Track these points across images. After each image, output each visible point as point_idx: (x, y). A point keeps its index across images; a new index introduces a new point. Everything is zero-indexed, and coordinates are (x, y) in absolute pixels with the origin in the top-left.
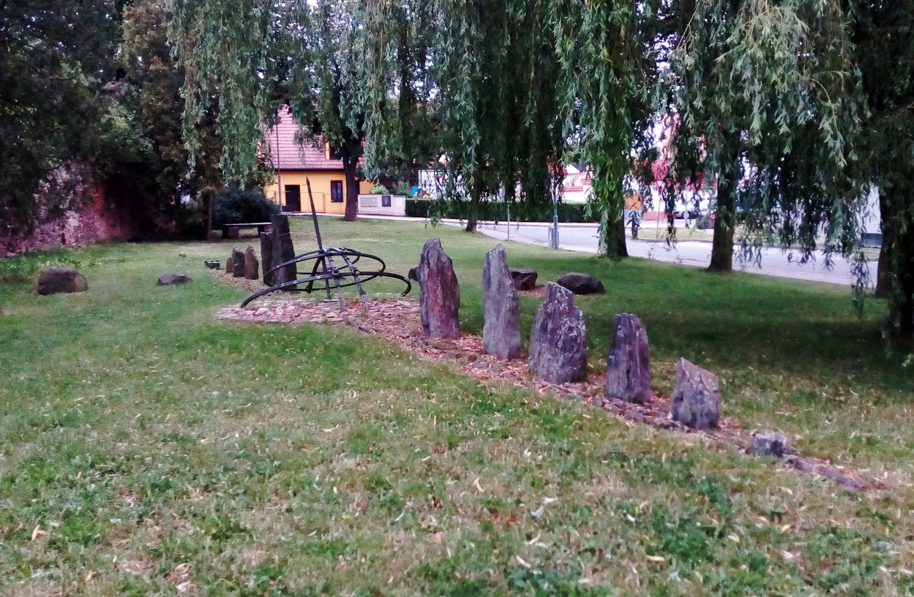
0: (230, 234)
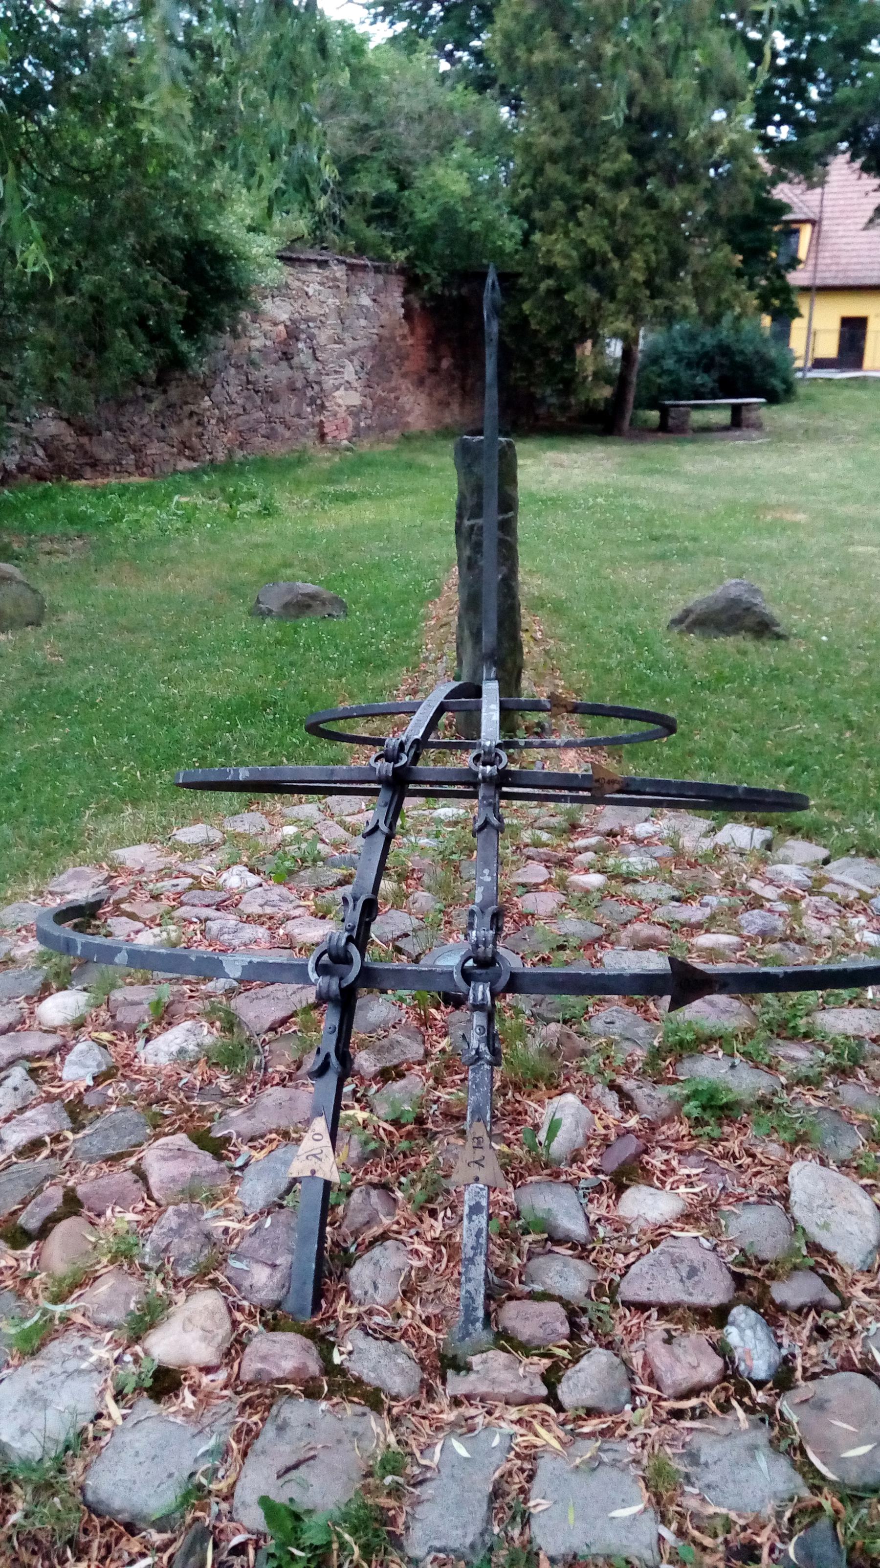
0: (671, 422)
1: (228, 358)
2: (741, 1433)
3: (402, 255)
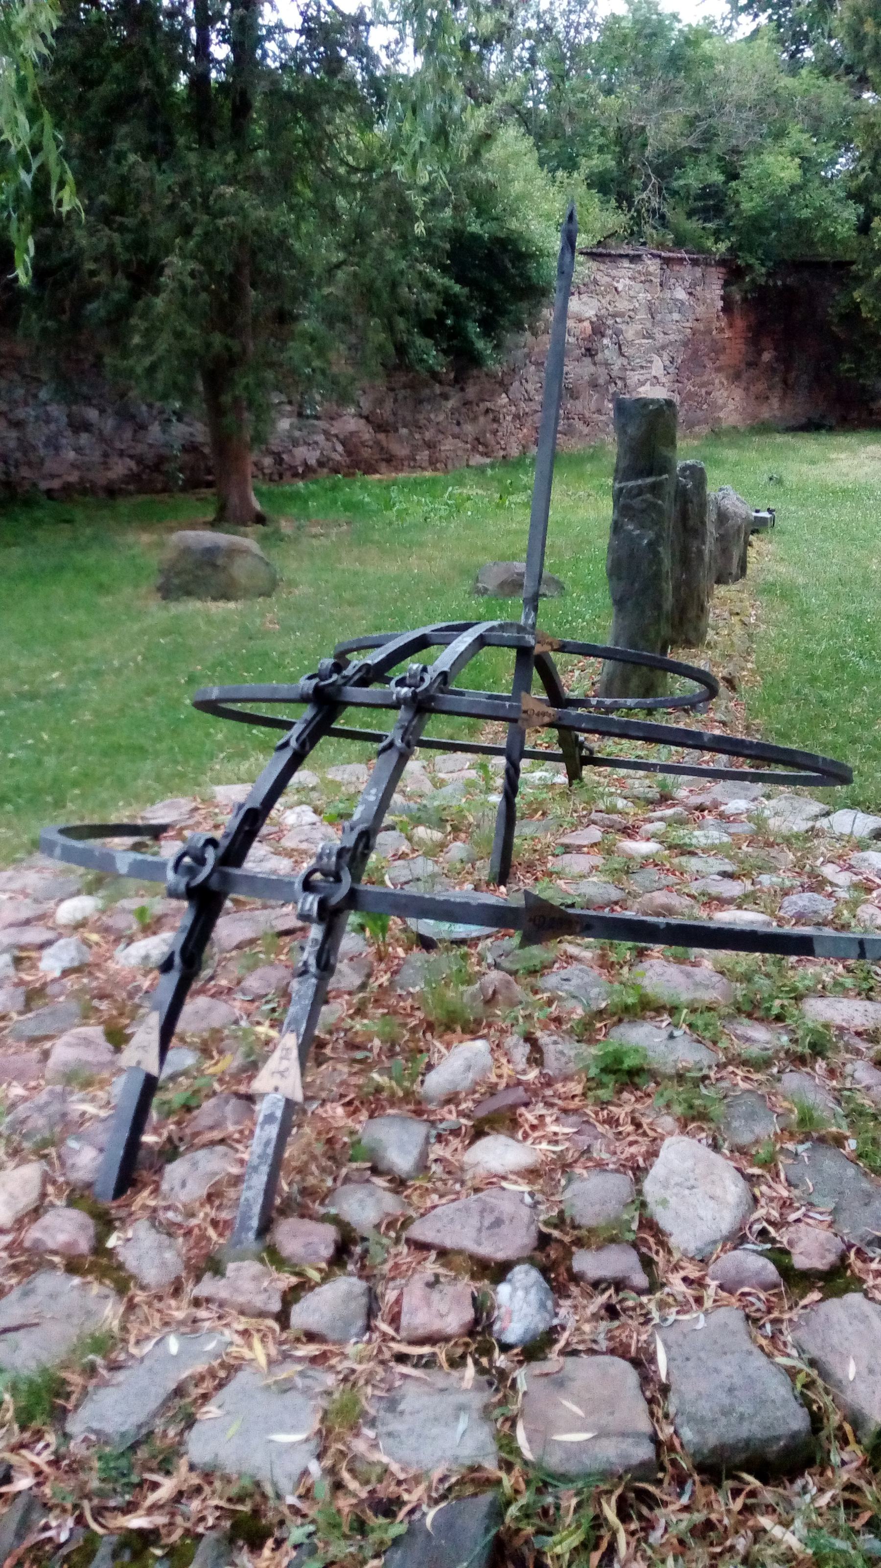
1: (528, 356)
2: (459, 1390)
3: (722, 247)
